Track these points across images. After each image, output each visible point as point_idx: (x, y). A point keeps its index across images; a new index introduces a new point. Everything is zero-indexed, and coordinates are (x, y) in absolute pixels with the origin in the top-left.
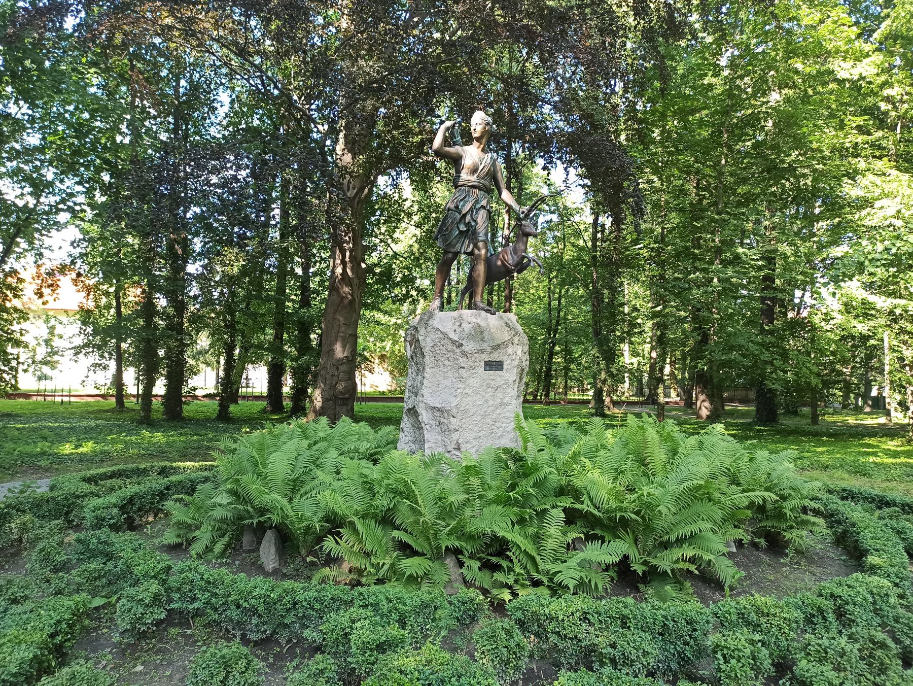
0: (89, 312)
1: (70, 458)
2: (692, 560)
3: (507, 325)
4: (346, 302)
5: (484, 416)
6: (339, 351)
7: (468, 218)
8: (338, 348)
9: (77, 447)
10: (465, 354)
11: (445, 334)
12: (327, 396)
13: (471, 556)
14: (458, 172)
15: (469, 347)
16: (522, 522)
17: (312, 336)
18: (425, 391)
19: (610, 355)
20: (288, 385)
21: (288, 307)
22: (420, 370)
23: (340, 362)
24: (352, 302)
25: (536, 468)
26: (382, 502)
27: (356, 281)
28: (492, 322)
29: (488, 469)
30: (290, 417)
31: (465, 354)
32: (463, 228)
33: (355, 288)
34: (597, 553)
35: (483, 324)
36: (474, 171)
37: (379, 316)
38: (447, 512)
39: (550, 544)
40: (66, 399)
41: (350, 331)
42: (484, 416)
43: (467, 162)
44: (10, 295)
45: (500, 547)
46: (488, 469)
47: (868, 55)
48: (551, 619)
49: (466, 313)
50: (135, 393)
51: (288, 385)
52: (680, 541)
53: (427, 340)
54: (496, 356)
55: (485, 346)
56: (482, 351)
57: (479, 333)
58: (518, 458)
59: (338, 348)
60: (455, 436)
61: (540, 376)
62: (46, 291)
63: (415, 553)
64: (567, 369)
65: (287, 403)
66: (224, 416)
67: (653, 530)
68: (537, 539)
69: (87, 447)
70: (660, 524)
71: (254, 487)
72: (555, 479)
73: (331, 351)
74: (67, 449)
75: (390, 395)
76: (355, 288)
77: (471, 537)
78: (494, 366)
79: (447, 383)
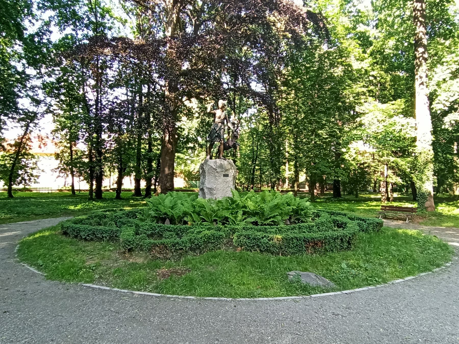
0: (58, 154)
1: (73, 211)
2: (272, 221)
3: (230, 163)
4: (170, 151)
5: (223, 190)
6: (167, 171)
7: (218, 132)
8: (166, 169)
9: (75, 207)
10: (217, 172)
11: (211, 166)
12: (163, 188)
13: (220, 222)
14: (215, 118)
15: (219, 170)
16: (232, 214)
17: (153, 164)
18: (206, 183)
19: (278, 171)
20: (143, 184)
21: (142, 152)
22: (204, 177)
23: (168, 175)
24: (172, 151)
25: (236, 201)
26: (197, 209)
27: (174, 143)
28: (225, 163)
29: (224, 202)
30: (145, 198)
31: (217, 172)
32: (216, 135)
33: (173, 145)
34: (249, 220)
35: (223, 163)
36: (220, 118)
37: (181, 156)
38: (214, 211)
39: (239, 219)
40: (50, 192)
41: (171, 163)
42: (223, 190)
43: (217, 115)
44: (28, 149)
45: (226, 219)
46: (224, 202)
47: (366, 59)
48: (236, 229)
49: (218, 160)
50: (75, 189)
51: (143, 184)
52: (270, 218)
53: (206, 168)
54: (226, 173)
55: (223, 170)
56: (222, 171)
57: (221, 166)
58: (232, 199)
59: (166, 169)
60: (215, 196)
61: (250, 180)
62: (42, 146)
63: (205, 221)
64: (261, 176)
65: (144, 193)
66: (118, 197)
67: (264, 216)
68: (235, 218)
69: (79, 207)
70: (266, 214)
71: (162, 208)
72: (241, 204)
73: (164, 171)
74: (72, 208)
75: (184, 189)
76: (173, 145)
77: (219, 218)
78: (226, 176)
79: (212, 181)
